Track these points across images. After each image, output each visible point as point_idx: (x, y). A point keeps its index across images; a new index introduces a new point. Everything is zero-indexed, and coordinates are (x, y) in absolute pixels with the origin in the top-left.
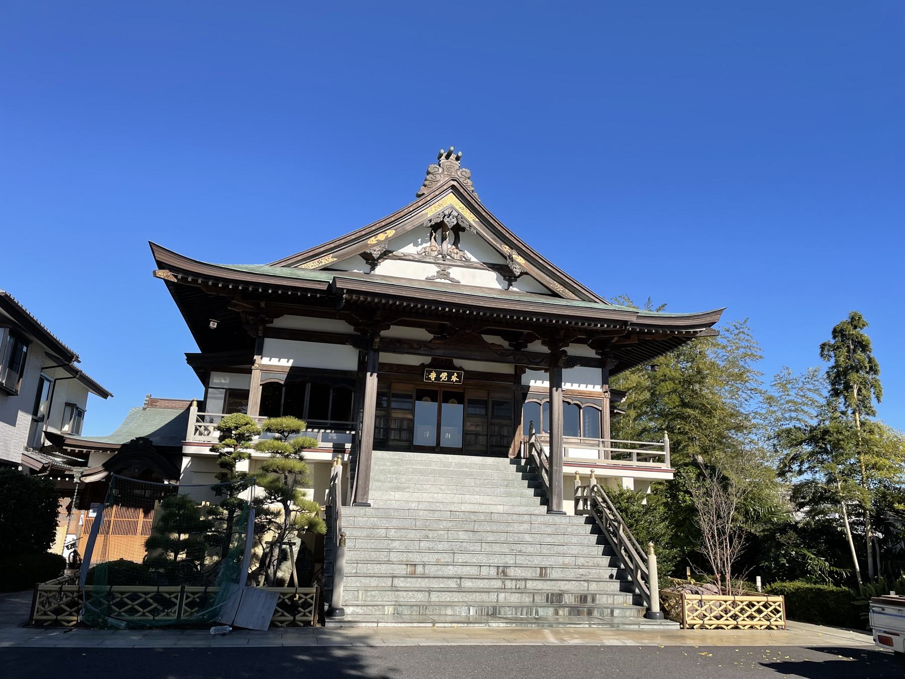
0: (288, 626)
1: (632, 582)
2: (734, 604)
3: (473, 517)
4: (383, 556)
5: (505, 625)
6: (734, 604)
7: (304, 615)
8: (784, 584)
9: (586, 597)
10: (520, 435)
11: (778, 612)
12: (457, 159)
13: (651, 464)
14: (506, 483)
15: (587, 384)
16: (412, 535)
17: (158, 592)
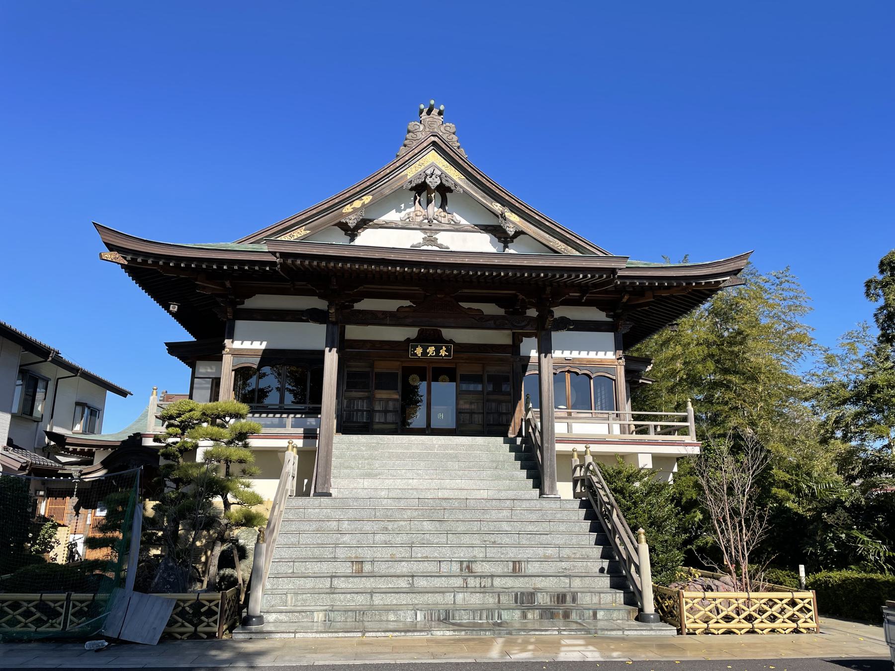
0: (188, 638)
1: (625, 577)
3: (444, 504)
4: (327, 553)
5: (451, 633)
7: (208, 625)
8: (831, 574)
9: (564, 596)
10: (520, 412)
11: (809, 611)
12: (440, 113)
13: (676, 437)
14: (495, 465)
15: (597, 351)
16: (368, 527)
17: (41, 600)
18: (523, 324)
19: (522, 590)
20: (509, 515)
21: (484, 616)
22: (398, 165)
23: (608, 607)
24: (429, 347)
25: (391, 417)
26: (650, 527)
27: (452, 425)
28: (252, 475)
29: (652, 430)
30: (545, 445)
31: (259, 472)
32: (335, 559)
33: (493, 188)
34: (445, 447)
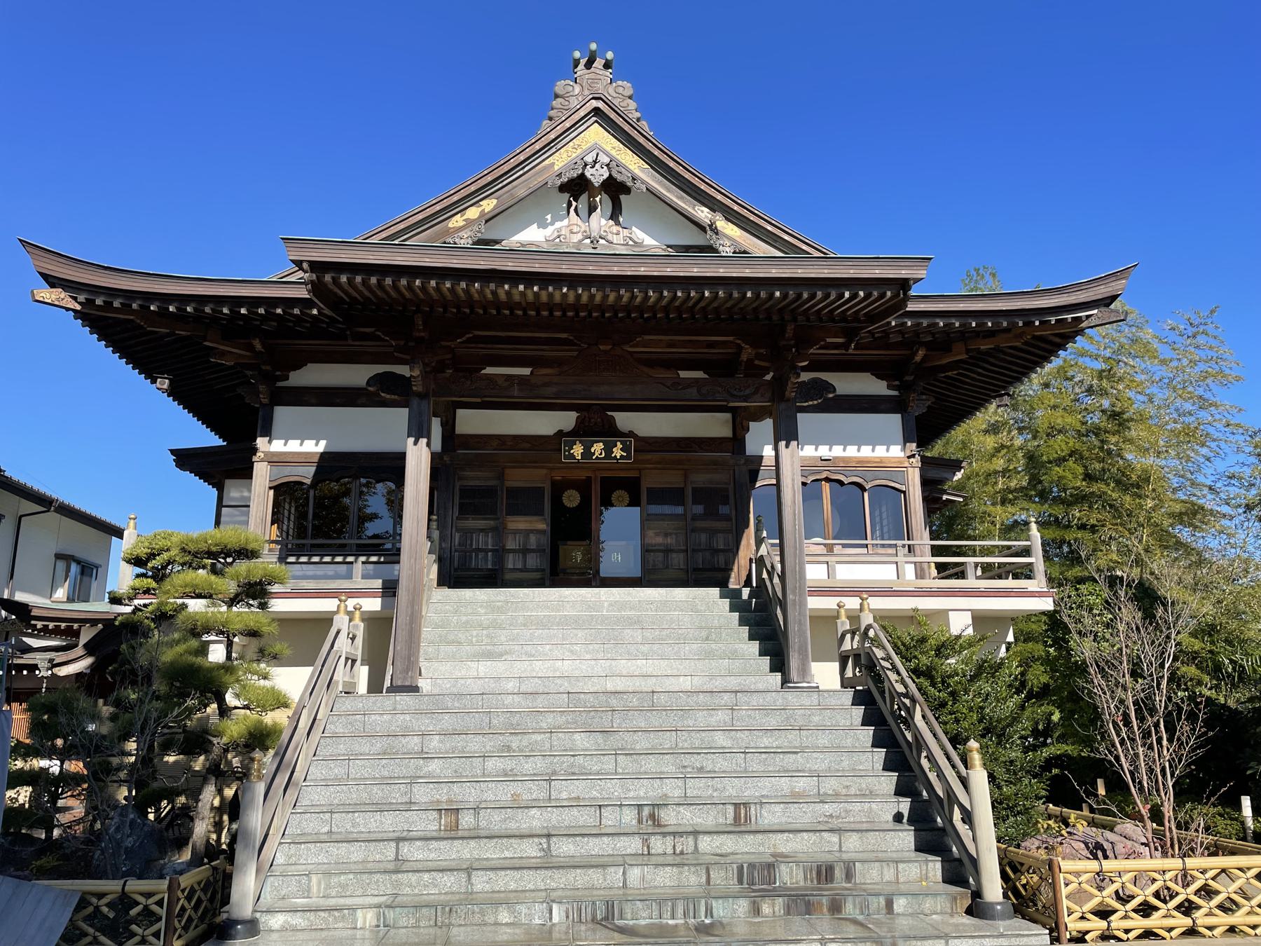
1: (943, 830)
2: (1185, 878)
3: (614, 702)
4: (397, 795)
6: (1185, 878)
9: (830, 869)
12: (607, 66)
13: (1010, 583)
14: (704, 634)
15: (874, 444)
18: (748, 392)
19: (753, 859)
20: (727, 718)
21: (680, 911)
22: (537, 147)
23: (914, 888)
24: (581, 423)
25: (533, 561)
26: (983, 736)
27: (636, 572)
28: (276, 659)
29: (970, 571)
30: (790, 597)
31: (287, 652)
32: (409, 806)
33: (696, 181)
34: (622, 606)
